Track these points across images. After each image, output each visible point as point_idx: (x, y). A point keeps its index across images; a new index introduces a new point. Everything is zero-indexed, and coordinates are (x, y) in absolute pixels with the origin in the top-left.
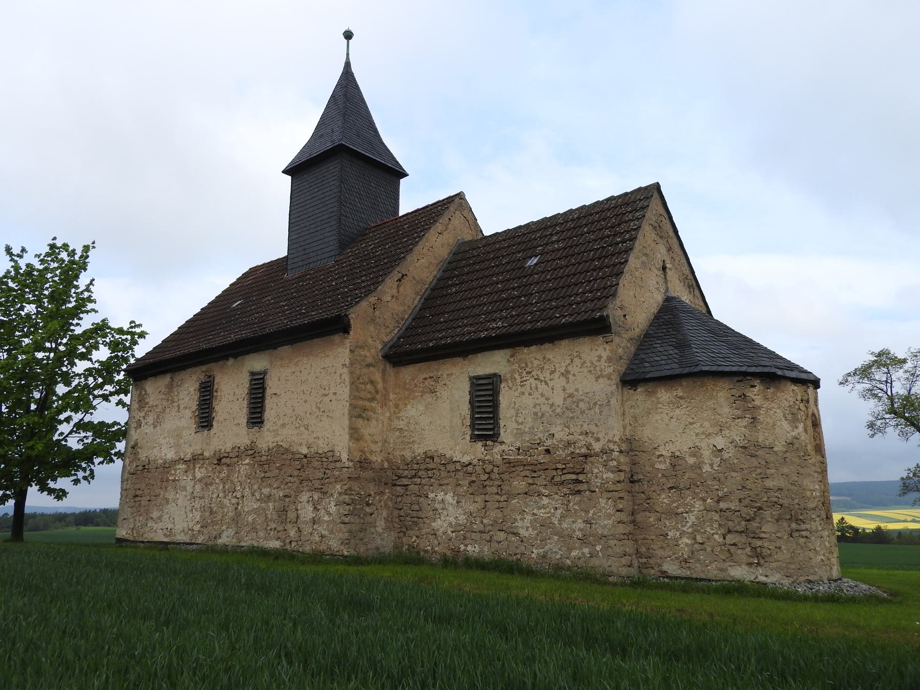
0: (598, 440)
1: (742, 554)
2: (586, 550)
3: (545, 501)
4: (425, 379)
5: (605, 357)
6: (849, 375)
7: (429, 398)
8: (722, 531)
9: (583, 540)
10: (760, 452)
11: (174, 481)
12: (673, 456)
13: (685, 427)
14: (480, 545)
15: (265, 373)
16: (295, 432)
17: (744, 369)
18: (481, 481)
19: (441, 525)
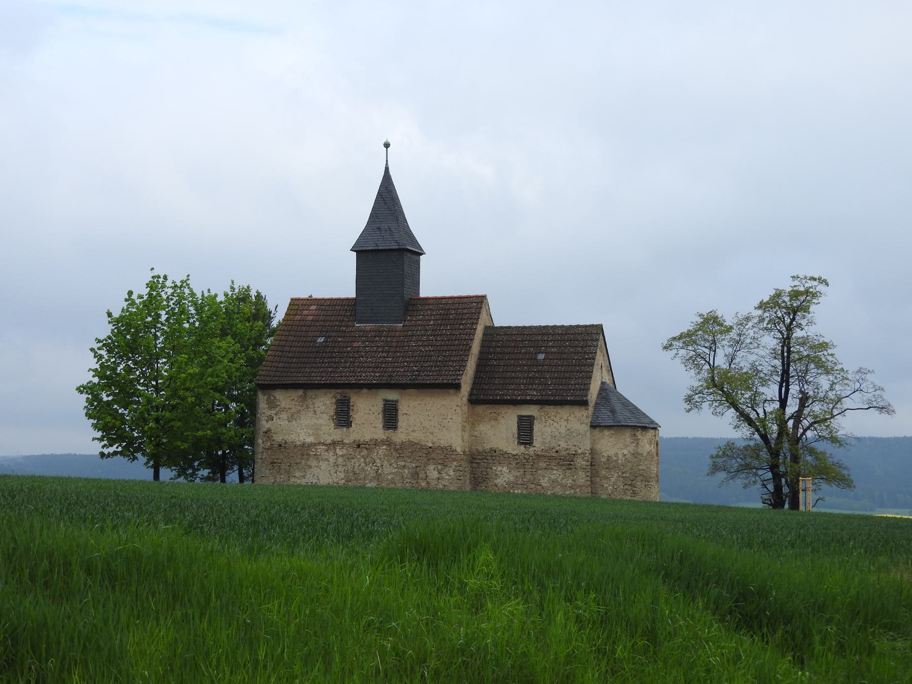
1: (629, 493)
6: (674, 339)
7: (493, 422)
11: (316, 455)
13: (612, 446)
15: (397, 401)
18: (520, 462)
19: (500, 481)
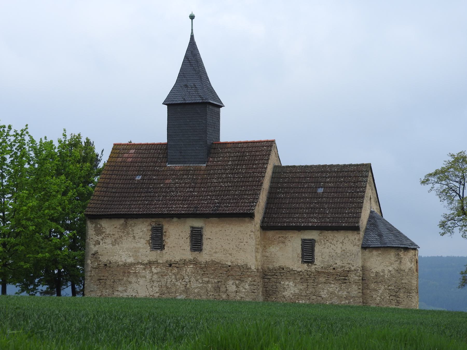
0: (353, 266)
1: (393, 302)
2: (347, 301)
3: (333, 285)
4: (280, 237)
5: (357, 239)
6: (430, 175)
7: (281, 245)
8: (389, 295)
9: (346, 298)
10: (401, 272)
12: (377, 272)
13: (380, 264)
14: (305, 300)
15: (202, 228)
16: (223, 256)
17: (399, 246)
18: (304, 278)
19: (287, 293)
